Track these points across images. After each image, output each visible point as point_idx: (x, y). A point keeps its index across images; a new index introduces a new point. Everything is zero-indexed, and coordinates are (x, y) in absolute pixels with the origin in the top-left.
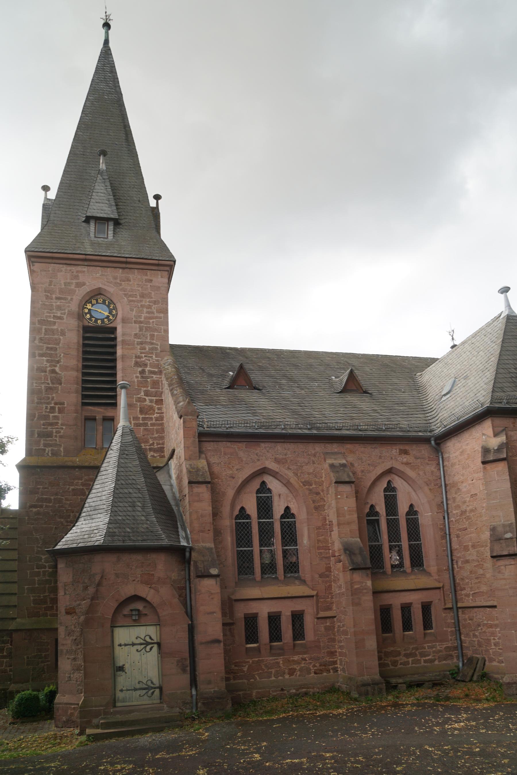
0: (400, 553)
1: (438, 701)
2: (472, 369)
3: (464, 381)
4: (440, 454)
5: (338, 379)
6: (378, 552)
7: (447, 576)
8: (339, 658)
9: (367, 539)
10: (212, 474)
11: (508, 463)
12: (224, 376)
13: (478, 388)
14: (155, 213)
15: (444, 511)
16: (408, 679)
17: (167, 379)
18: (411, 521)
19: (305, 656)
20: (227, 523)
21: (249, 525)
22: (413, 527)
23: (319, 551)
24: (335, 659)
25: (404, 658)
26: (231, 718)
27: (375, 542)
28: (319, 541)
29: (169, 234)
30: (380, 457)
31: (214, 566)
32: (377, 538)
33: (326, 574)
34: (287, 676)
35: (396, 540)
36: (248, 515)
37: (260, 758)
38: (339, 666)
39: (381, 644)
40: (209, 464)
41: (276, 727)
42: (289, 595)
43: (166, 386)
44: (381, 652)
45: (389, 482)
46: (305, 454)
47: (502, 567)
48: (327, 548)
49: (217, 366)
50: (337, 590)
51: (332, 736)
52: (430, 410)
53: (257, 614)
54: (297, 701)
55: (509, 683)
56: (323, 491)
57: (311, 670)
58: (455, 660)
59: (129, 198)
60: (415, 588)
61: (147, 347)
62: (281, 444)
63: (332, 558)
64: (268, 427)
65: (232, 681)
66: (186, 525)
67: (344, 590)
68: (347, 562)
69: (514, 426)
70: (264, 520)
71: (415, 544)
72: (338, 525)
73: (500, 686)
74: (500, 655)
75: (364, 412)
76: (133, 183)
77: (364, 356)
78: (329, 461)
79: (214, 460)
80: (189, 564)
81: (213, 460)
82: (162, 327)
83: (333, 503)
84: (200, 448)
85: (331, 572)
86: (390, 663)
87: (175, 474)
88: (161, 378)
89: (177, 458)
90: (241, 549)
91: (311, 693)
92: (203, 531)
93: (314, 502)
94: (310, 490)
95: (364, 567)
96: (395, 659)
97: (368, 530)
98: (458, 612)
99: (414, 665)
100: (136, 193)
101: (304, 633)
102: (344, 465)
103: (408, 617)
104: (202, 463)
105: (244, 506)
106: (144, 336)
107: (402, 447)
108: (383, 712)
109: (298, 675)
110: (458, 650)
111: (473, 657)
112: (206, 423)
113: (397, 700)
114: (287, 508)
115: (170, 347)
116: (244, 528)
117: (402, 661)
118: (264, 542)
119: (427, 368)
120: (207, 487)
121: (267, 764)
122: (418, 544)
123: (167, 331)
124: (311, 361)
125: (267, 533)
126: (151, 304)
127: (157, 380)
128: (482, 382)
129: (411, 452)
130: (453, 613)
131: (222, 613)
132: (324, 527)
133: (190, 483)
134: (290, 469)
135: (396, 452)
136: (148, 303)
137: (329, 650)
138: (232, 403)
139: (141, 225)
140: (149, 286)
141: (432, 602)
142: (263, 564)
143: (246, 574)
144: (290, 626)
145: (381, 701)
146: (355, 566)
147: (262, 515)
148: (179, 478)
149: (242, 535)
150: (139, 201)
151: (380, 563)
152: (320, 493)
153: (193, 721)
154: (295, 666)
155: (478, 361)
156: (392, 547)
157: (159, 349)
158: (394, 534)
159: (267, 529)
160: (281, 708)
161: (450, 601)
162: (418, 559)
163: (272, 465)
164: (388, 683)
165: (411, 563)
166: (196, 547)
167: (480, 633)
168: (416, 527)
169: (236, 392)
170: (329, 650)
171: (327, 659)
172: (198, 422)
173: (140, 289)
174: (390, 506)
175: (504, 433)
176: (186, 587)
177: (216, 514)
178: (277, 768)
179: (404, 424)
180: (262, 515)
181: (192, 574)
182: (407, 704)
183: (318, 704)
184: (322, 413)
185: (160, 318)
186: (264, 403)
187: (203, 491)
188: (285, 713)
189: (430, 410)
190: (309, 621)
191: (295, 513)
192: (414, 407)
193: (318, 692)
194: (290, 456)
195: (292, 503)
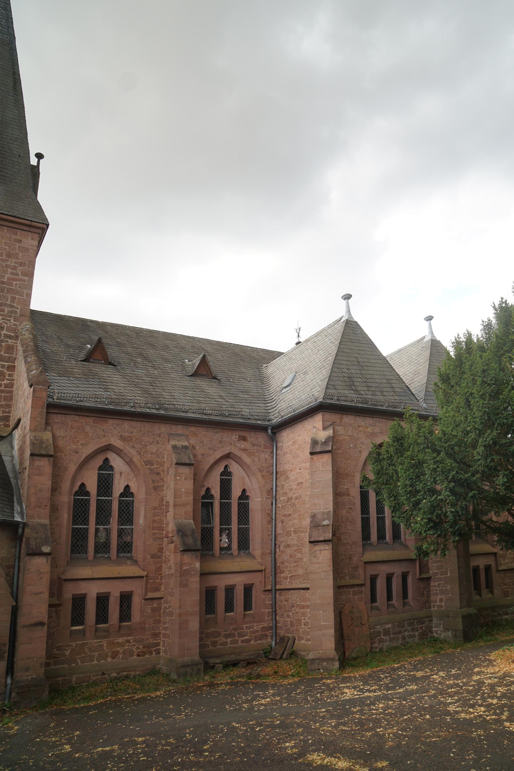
0: (229, 536)
1: (250, 679)
2: (311, 366)
3: (303, 376)
4: (275, 443)
5: (190, 363)
6: (209, 535)
7: (270, 559)
8: (163, 639)
9: (200, 521)
10: (56, 447)
11: (332, 456)
12: (81, 348)
13: (314, 384)
14: (35, 172)
15: (273, 497)
16: (225, 659)
17: (22, 345)
18: (242, 505)
19: (130, 638)
20: (66, 499)
21: (88, 501)
22: (244, 511)
23: (153, 532)
24: (159, 641)
25: (223, 638)
26: (45, 707)
27: (207, 524)
28: (154, 521)
29: (47, 196)
30: (221, 442)
31: (46, 544)
32: (210, 520)
33: (158, 555)
34: (109, 660)
35: (227, 523)
36: (88, 492)
37: (70, 749)
38: (161, 648)
39: (204, 625)
40: (54, 437)
41: (92, 714)
42: (120, 576)
43: (21, 353)
44: (203, 633)
45: (226, 467)
46: (150, 434)
47: (318, 552)
48: (161, 529)
49: (76, 338)
50: (167, 571)
51: (147, 720)
52: (271, 401)
53: (86, 594)
54: (116, 685)
55: (312, 659)
56: (163, 471)
57: (134, 652)
58: (269, 640)
59: (8, 151)
60: (240, 570)
61: (6, 309)
62: (128, 422)
63: (165, 539)
64: (118, 404)
65: (52, 667)
66: (23, 499)
67: (173, 571)
68: (179, 543)
69: (341, 422)
70: (103, 498)
71: (244, 528)
72: (174, 506)
73: (305, 663)
74: (308, 633)
75: (211, 397)
76: (15, 136)
77: (218, 342)
78: (173, 442)
79: (60, 433)
80: (21, 541)
81: (58, 433)
82: (25, 291)
83: (172, 484)
84: (47, 419)
85: (162, 552)
86: (210, 644)
87: (18, 445)
88: (17, 343)
89: (22, 429)
90: (77, 526)
91: (132, 676)
92: (39, 507)
93: (153, 481)
94: (151, 470)
95: (194, 548)
96: (215, 639)
97: (202, 512)
98: (276, 594)
99: (232, 645)
100: (17, 147)
101: (130, 615)
102: (186, 447)
103: (231, 599)
104: (47, 436)
105: (85, 483)
106: (4, 297)
107: (241, 433)
108: (199, 692)
109: (120, 658)
110: (272, 630)
111: (285, 636)
112: (57, 394)
113: (213, 680)
114: (127, 487)
115: (31, 312)
116: (82, 505)
117: (221, 642)
118: (100, 521)
119: (272, 360)
120: (49, 461)
121: (77, 755)
122: (246, 528)
123: (29, 296)
124: (168, 342)
125: (104, 511)
126: (16, 265)
127: (12, 345)
128: (318, 378)
129: (249, 439)
130: (272, 594)
131: (50, 594)
132: (161, 508)
133: (32, 455)
134: (134, 448)
135: (236, 438)
136: (13, 264)
137: (153, 631)
138: (85, 377)
139: (17, 181)
140: (17, 246)
141: (253, 584)
142: (97, 542)
143: (79, 553)
144: (118, 608)
145: (198, 682)
146: (186, 548)
147: (101, 493)
148: (22, 450)
149: (80, 512)
150: (19, 156)
151: (210, 545)
152: (160, 474)
153: (4, 714)
154: (118, 649)
155: (317, 359)
156: (223, 530)
157: (19, 313)
158: (226, 517)
159: (104, 507)
160: (100, 693)
161: (270, 583)
162: (245, 542)
163: (117, 443)
164: (206, 663)
165: (239, 547)
166: (30, 523)
167: (293, 614)
168: (246, 511)
169: (91, 366)
170: (153, 631)
171: (151, 641)
172: (49, 393)
173: (7, 248)
174: (224, 490)
175: (332, 427)
176: (14, 565)
177: (55, 489)
178: (86, 759)
179: (246, 411)
180: (101, 493)
181: (22, 551)
182: (222, 684)
183: (138, 687)
184: (172, 394)
185: (25, 281)
186: (117, 379)
187: (45, 464)
188: (103, 698)
189: (271, 401)
190: (137, 601)
191: (134, 492)
192: (257, 396)
193: (139, 675)
194: (136, 434)
195: (132, 482)
